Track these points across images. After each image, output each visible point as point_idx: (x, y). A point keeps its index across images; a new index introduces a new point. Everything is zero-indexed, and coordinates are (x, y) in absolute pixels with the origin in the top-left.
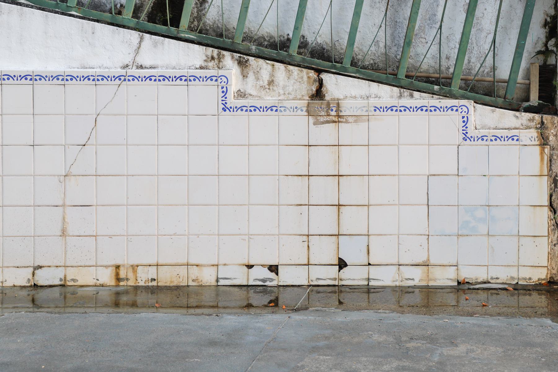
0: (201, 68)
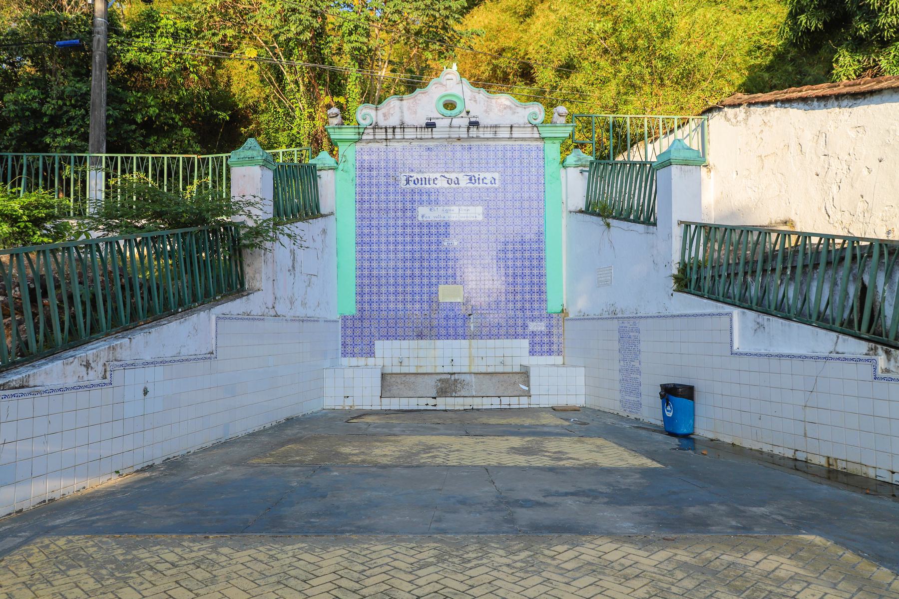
0: (866, 354)
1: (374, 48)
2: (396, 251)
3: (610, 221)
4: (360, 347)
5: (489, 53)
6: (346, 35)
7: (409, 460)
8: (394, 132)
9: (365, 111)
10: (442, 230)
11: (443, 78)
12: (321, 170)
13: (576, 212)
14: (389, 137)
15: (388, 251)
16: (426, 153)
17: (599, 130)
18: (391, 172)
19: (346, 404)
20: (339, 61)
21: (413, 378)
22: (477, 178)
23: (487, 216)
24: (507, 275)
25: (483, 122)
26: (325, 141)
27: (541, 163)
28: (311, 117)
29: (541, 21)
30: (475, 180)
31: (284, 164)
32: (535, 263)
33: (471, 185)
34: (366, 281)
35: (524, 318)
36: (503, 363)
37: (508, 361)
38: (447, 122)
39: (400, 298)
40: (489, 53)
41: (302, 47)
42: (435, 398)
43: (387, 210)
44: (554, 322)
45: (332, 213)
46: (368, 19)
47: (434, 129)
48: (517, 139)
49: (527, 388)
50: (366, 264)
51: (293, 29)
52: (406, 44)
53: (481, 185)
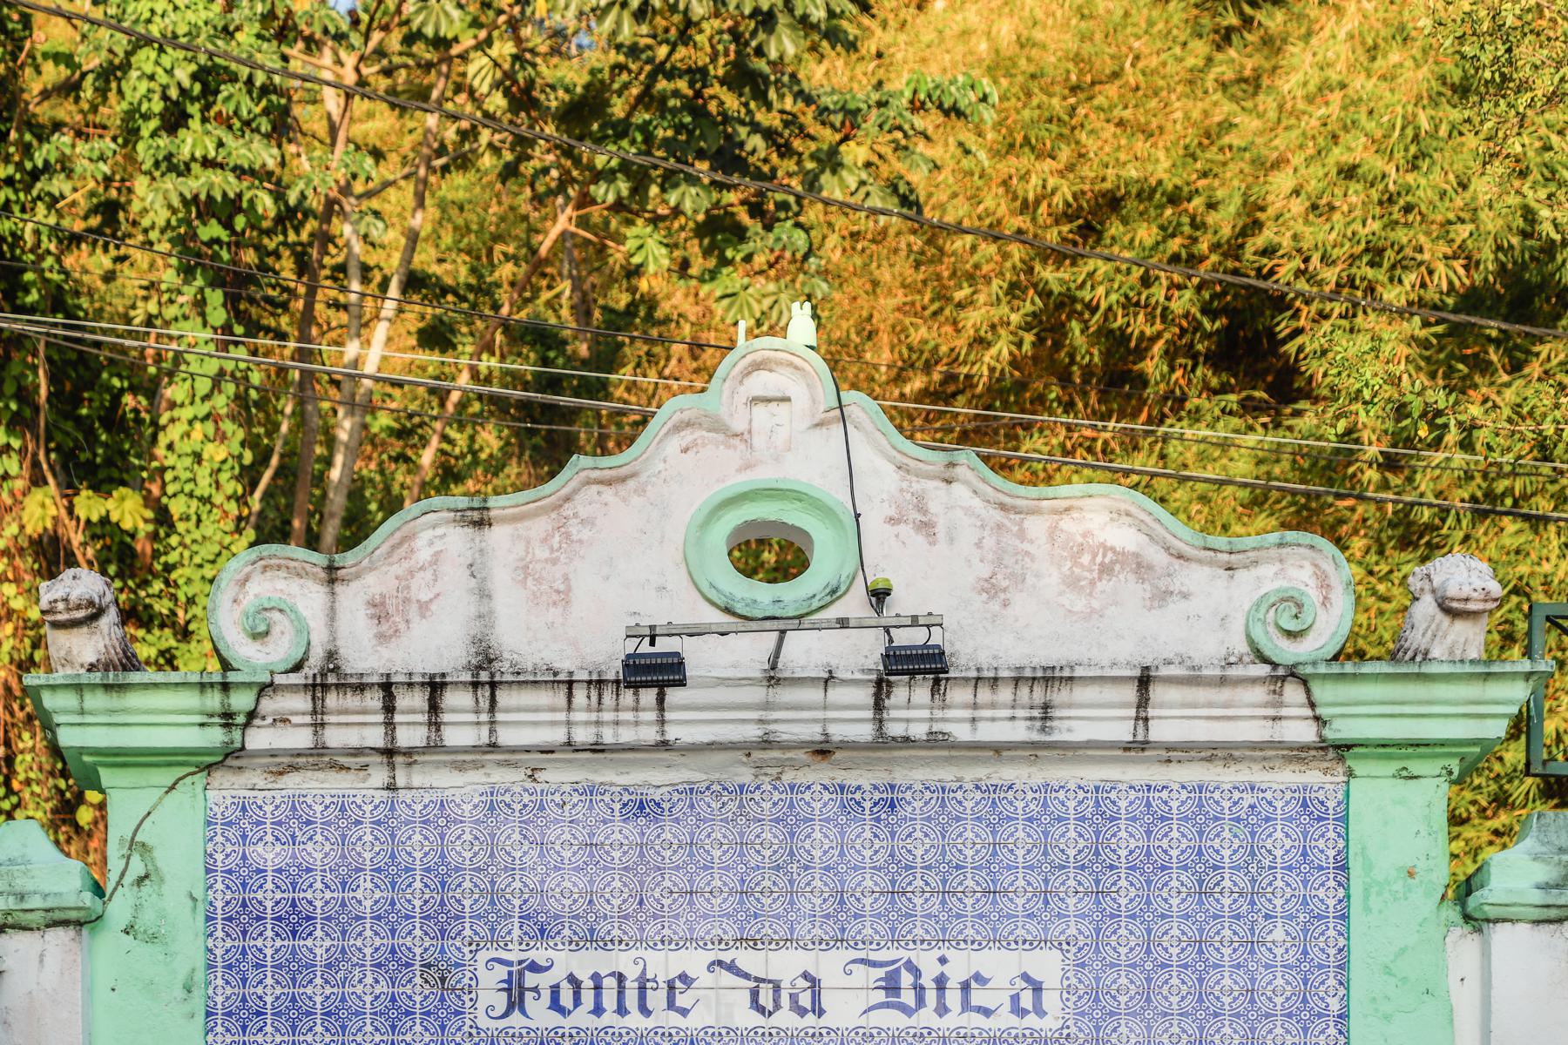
6: (147, 128)
8: (434, 708)
9: (263, 588)
14: (411, 735)
16: (622, 833)
18: (417, 942)
22: (927, 981)
30: (919, 990)
33: (892, 1020)
38: (751, 650)
47: (674, 695)
48: (1176, 752)
52: (510, 172)
53: (953, 1020)
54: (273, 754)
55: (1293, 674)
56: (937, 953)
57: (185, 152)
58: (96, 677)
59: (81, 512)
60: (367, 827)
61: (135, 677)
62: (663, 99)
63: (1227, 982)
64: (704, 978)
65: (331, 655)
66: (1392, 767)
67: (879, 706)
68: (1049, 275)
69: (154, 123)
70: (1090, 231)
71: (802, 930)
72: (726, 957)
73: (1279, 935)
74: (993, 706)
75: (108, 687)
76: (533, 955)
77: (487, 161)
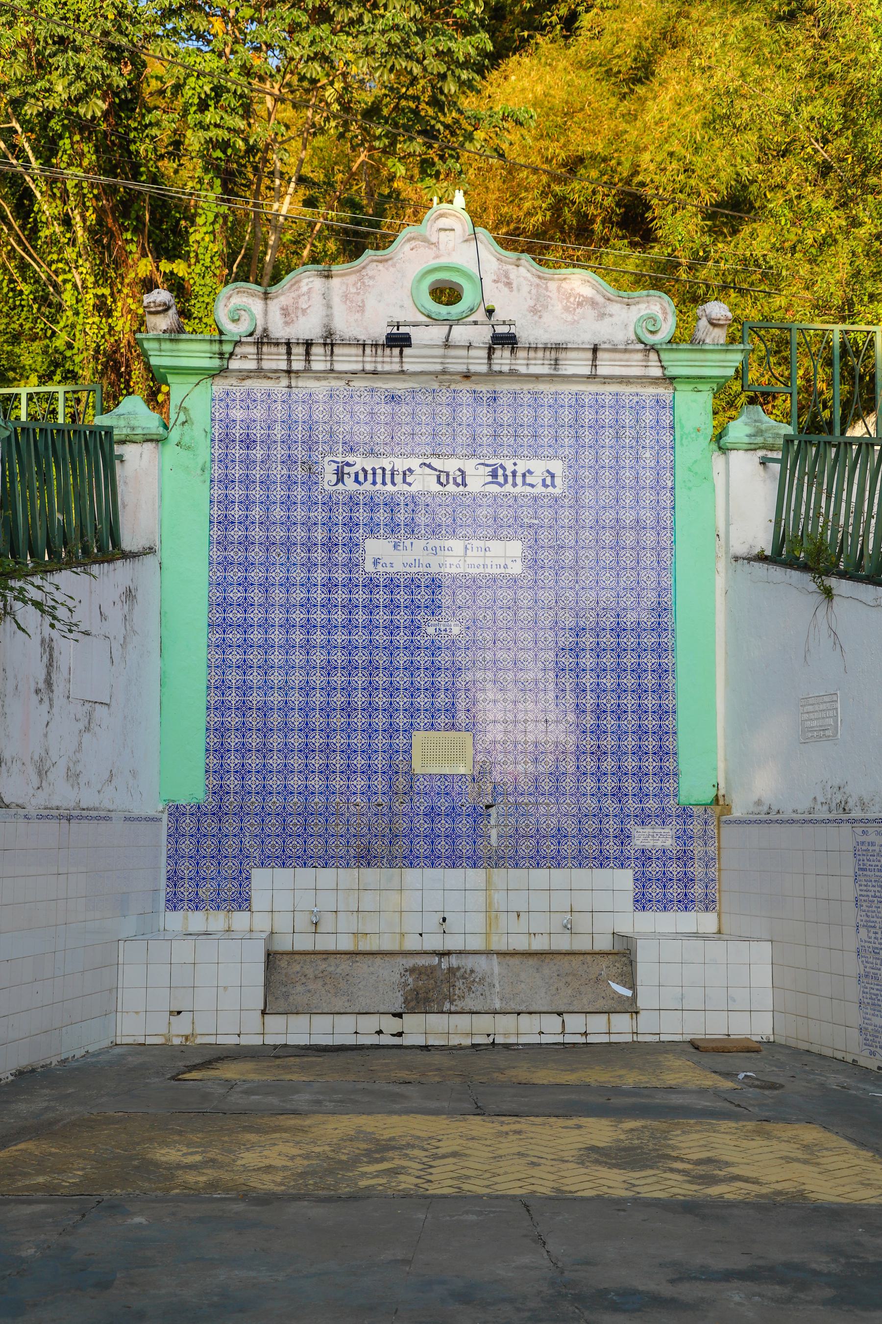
1: (261, 145)
2: (308, 647)
3: (832, 582)
4: (215, 884)
5: (545, 167)
7: (330, 1180)
8: (308, 354)
9: (237, 300)
10: (423, 597)
11: (429, 226)
12: (123, 442)
13: (749, 559)
14: (297, 365)
15: (288, 647)
16: (387, 408)
17: (807, 362)
18: (299, 453)
19: (175, 1030)
20: (176, 172)
21: (344, 966)
22: (509, 473)
23: (533, 563)
24: (580, 710)
25: (526, 333)
26: (137, 368)
27: (667, 439)
28: (103, 309)
29: (671, 93)
30: (505, 476)
31: (31, 426)
32: (649, 681)
33: (494, 488)
34: (234, 720)
35: (622, 816)
36: (569, 928)
37: (583, 923)
38: (437, 333)
39: (317, 762)
40: (545, 167)
41: (81, 133)
42: (399, 1015)
43: (288, 545)
44: (696, 827)
45: (150, 550)
46: (247, 71)
47: (406, 351)
49: (628, 993)
50: (234, 677)
51: (59, 88)
52: (341, 136)
53: (519, 489)
54: (240, 371)
55: (653, 348)
56: (512, 461)
57: (208, 120)
58: (167, 336)
59: (162, 269)
60: (279, 403)
61: (183, 336)
62: (403, 110)
63: (628, 474)
64: (418, 470)
65: (265, 330)
66: (691, 387)
67: (489, 358)
68: (557, 188)
69: (194, 108)
70: (572, 171)
71: (458, 450)
72: (427, 462)
73: (648, 455)
74: (535, 359)
75: (171, 340)
76: (348, 459)
77: (332, 131)
